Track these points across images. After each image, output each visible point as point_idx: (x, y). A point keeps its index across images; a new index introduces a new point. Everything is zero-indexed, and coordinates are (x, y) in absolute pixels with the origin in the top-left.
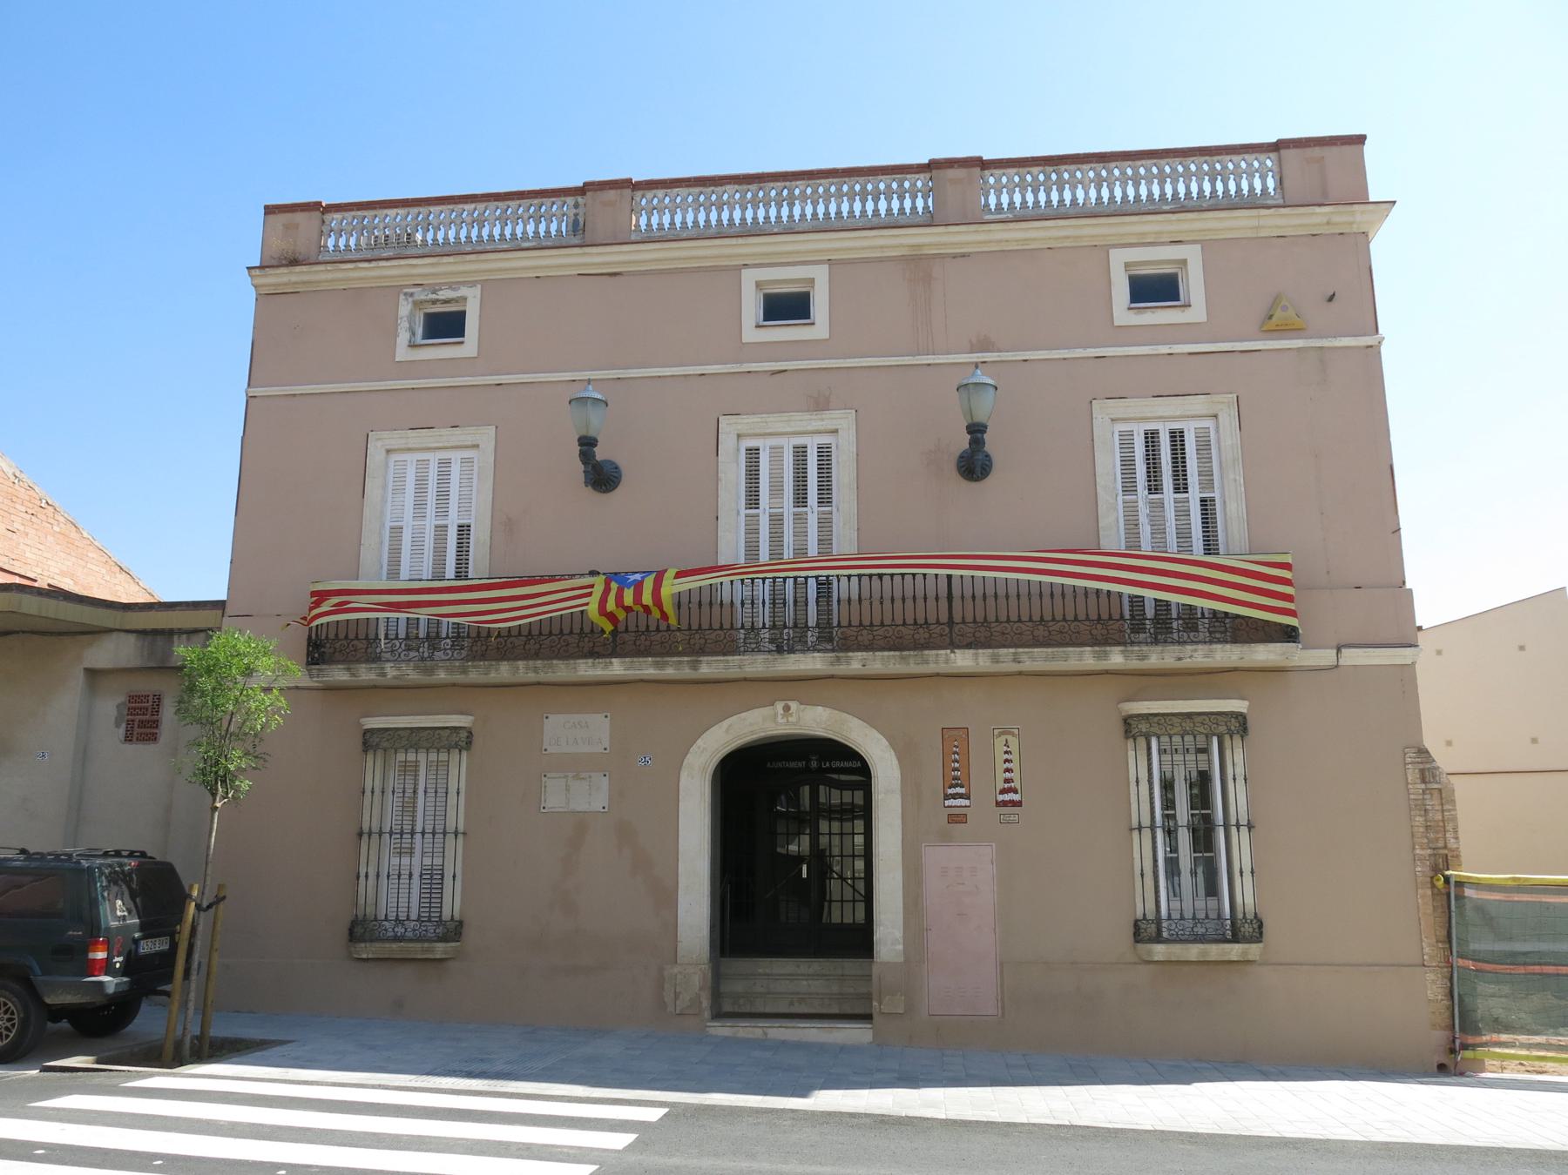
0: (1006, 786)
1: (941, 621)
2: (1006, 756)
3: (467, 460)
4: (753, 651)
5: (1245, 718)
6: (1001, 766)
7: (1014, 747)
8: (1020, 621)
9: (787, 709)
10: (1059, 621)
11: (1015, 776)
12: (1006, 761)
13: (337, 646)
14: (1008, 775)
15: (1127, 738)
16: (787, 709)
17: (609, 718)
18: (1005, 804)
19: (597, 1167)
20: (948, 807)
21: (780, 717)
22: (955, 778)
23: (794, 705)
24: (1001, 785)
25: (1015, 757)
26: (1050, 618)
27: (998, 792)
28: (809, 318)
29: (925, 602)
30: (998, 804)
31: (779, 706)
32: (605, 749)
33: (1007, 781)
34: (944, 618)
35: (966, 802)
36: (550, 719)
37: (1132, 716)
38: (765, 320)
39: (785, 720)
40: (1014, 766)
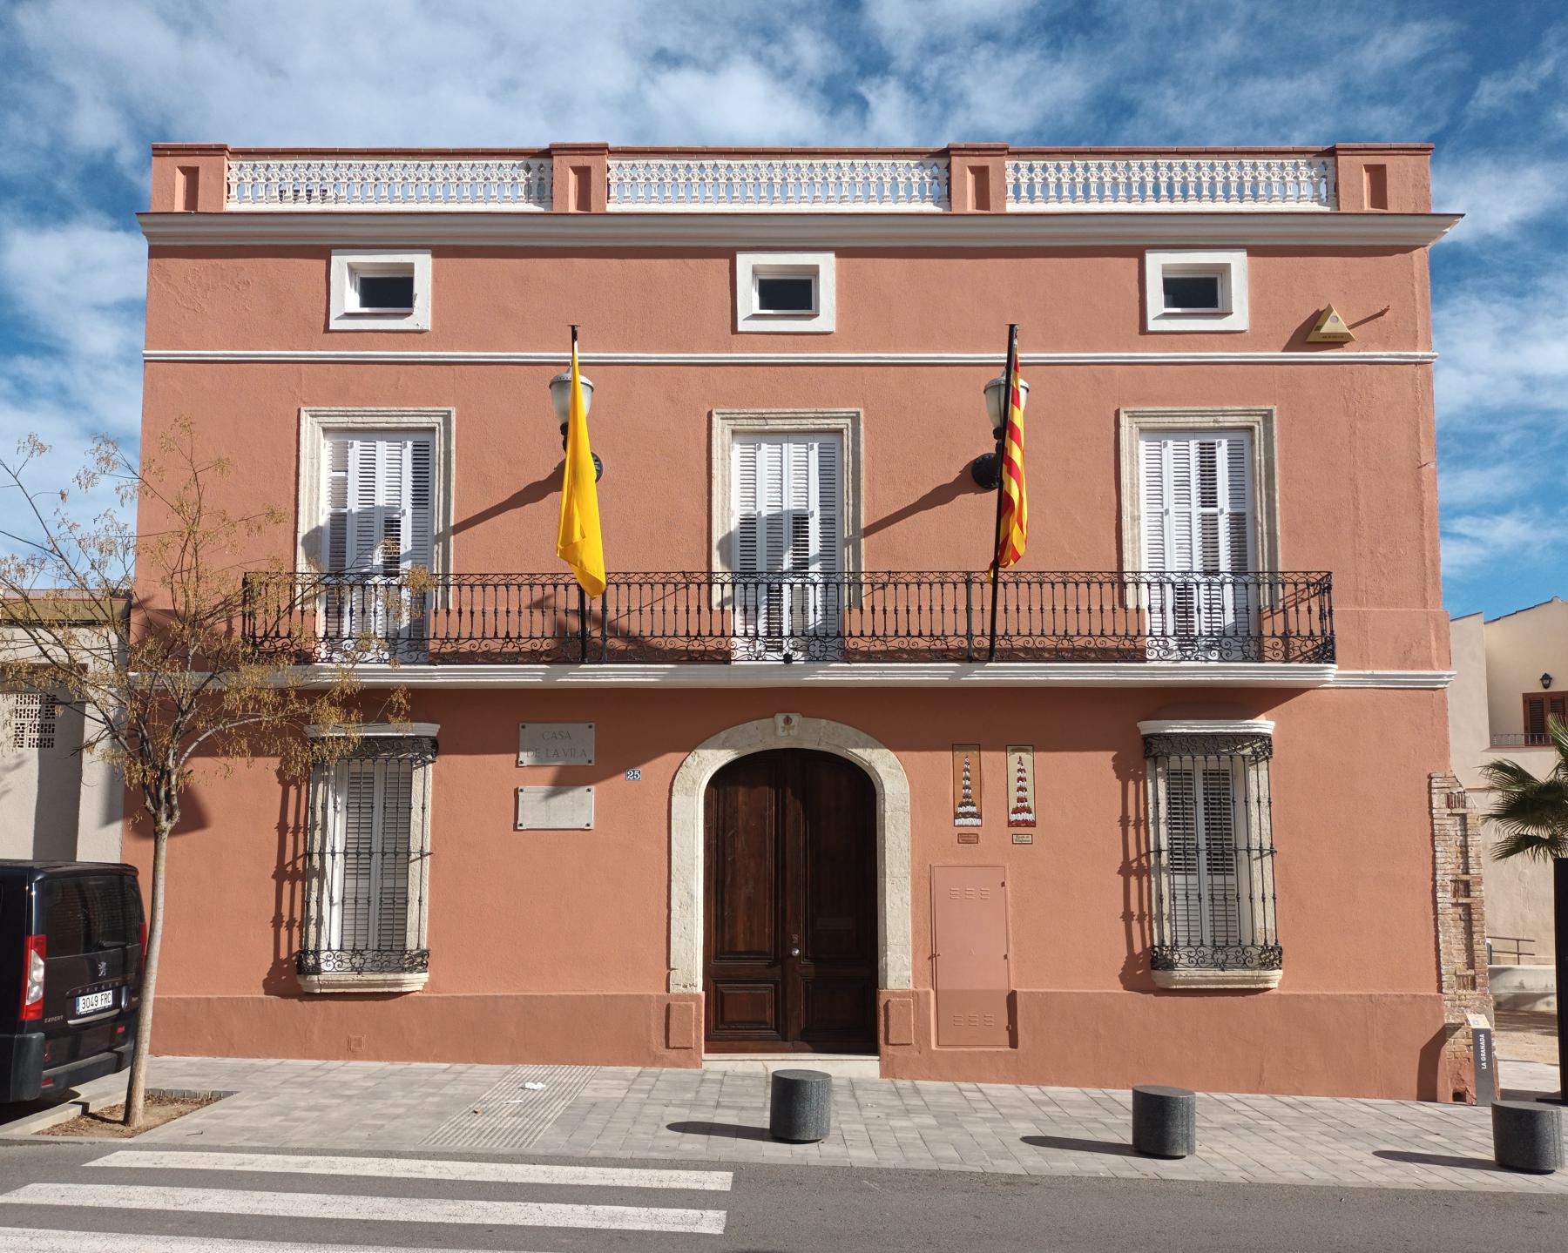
0: (1019, 805)
1: (959, 633)
2: (1020, 774)
3: (799, 415)
4: (818, 660)
5: (1270, 740)
6: (1014, 784)
7: (1028, 765)
8: (1042, 635)
9: (788, 721)
10: (282, 638)
11: (1029, 794)
12: (1020, 779)
13: (279, 644)
14: (1021, 794)
15: (1146, 758)
16: (788, 721)
17: (593, 729)
18: (1018, 824)
19: (73, 1089)
20: (959, 826)
21: (780, 730)
22: (966, 796)
23: (795, 718)
24: (1013, 804)
25: (1028, 775)
26: (708, 634)
27: (1010, 811)
28: (811, 309)
29: (460, 616)
30: (1011, 824)
31: (780, 718)
32: (590, 762)
33: (1020, 800)
34: (962, 630)
35: (978, 822)
36: (527, 728)
37: (1151, 736)
38: (762, 307)
39: (786, 733)
40: (1028, 784)
